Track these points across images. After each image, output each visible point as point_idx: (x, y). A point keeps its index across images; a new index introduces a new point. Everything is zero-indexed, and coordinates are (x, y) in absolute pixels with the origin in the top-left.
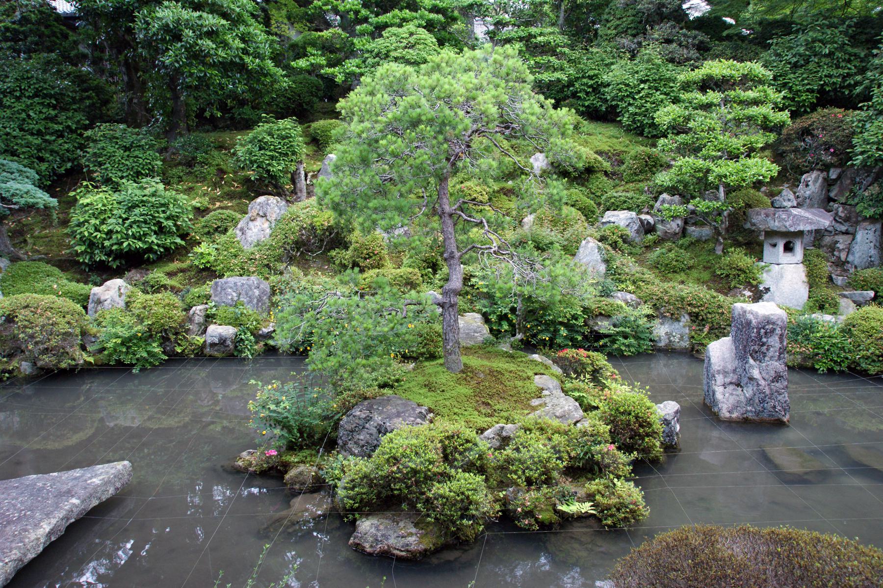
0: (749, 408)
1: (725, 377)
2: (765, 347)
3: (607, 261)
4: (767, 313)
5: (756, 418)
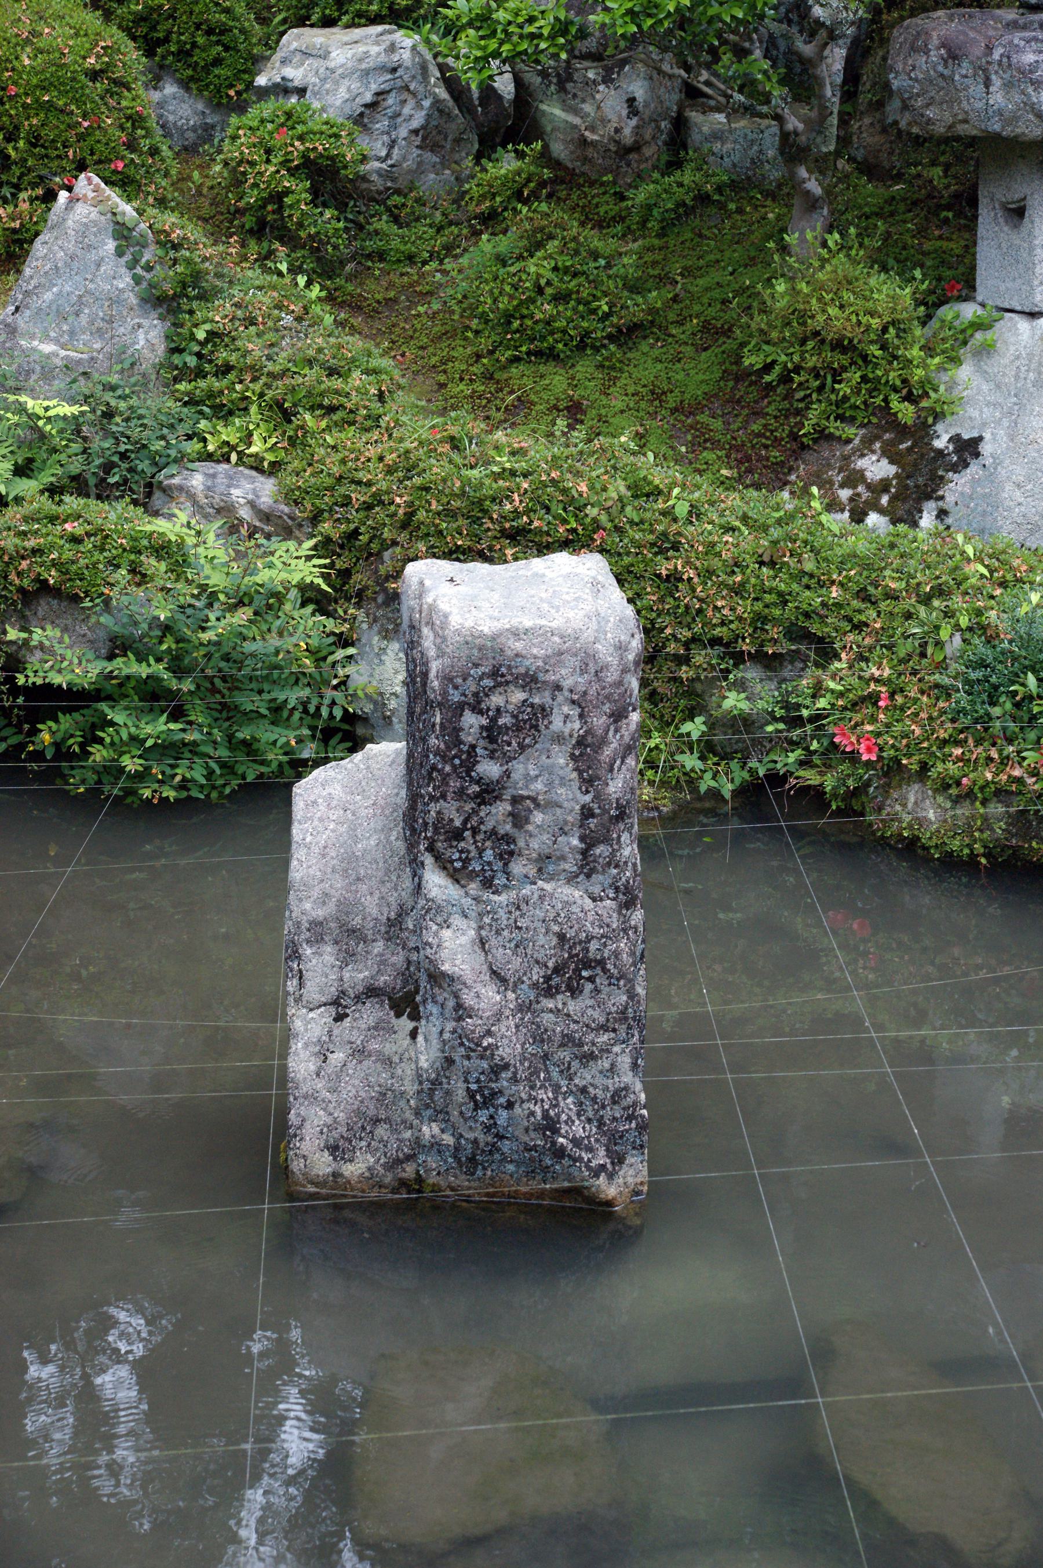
0: (429, 1130)
1: (348, 957)
2: (502, 808)
3: (168, 303)
4: (487, 628)
5: (461, 1180)
